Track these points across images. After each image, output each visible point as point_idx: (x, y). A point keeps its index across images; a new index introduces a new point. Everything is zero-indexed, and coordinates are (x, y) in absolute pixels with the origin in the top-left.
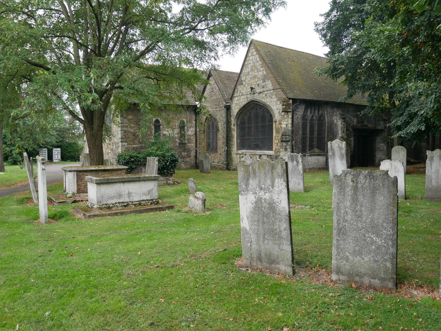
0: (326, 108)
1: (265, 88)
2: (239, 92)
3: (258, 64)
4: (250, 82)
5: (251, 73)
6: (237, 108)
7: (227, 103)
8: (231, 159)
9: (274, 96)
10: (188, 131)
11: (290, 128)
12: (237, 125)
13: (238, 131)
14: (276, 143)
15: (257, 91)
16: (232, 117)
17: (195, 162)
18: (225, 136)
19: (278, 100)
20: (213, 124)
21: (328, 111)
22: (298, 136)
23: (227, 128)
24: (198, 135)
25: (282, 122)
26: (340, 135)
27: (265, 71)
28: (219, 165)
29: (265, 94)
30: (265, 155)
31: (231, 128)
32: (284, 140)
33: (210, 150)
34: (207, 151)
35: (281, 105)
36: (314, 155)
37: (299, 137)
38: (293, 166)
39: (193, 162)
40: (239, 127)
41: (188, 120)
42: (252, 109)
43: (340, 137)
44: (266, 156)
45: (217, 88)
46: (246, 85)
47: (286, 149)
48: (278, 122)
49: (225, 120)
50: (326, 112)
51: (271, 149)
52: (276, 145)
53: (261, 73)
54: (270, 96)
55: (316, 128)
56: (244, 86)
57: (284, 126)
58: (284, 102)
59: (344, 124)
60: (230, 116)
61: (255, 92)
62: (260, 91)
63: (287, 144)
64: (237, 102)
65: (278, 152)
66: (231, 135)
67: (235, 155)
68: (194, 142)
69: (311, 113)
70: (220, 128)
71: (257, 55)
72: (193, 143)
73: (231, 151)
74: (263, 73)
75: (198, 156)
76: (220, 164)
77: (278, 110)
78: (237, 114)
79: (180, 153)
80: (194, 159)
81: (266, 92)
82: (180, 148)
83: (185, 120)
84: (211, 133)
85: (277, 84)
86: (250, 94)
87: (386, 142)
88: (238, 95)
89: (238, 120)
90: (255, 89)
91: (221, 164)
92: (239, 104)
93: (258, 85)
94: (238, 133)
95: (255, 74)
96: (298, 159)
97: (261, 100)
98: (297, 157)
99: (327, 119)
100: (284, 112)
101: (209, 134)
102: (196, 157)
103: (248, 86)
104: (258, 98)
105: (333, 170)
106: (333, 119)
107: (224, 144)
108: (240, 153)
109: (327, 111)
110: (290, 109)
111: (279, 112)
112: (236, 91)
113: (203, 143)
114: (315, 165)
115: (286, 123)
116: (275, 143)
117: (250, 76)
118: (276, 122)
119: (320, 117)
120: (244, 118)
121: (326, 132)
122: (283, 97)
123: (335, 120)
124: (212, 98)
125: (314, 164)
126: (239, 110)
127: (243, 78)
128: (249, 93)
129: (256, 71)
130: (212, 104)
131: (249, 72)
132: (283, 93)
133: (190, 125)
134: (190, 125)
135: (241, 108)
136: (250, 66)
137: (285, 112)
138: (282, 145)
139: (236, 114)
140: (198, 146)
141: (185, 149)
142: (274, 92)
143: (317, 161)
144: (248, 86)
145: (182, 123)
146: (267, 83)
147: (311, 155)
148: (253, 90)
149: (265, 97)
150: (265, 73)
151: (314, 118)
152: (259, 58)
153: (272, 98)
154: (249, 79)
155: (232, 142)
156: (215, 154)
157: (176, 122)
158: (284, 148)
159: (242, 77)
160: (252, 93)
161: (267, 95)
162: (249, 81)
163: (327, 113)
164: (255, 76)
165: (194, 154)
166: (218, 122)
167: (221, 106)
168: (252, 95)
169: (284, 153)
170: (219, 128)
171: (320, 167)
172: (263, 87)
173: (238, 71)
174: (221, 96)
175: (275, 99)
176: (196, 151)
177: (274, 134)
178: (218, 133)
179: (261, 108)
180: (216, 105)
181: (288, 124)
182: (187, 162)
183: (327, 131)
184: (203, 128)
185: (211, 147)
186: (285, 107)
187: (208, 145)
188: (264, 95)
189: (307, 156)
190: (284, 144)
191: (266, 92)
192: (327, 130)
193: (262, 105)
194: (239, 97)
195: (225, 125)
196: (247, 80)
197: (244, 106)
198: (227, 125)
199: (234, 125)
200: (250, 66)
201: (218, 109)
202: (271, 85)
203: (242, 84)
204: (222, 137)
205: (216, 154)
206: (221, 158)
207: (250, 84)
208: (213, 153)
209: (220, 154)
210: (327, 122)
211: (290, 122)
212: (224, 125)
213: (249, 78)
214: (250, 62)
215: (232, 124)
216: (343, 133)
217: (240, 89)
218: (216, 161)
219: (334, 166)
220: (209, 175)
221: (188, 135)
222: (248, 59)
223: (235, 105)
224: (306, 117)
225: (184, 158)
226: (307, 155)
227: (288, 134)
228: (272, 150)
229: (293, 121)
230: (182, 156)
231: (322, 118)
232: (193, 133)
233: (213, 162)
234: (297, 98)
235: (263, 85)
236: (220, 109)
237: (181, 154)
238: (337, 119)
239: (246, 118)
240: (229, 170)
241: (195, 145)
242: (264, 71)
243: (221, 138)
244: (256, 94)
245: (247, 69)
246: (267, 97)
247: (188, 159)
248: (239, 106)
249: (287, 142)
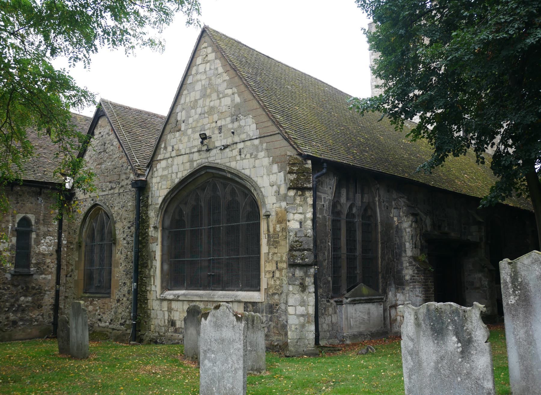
0: (378, 189)
1: (239, 135)
2: (170, 149)
3: (219, 81)
4: (200, 124)
5: (200, 102)
6: (163, 187)
7: (139, 175)
8: (146, 312)
9: (262, 154)
10: (38, 243)
11: (310, 232)
12: (163, 229)
13: (166, 243)
14: (269, 272)
15: (218, 144)
16: (150, 208)
17: (52, 320)
18: (131, 255)
19: (274, 162)
20: (103, 227)
21: (382, 198)
22: (324, 254)
23: (137, 236)
24: (64, 255)
25: (291, 216)
26: (409, 253)
27: (239, 96)
28: (114, 327)
29: (237, 150)
30: (239, 302)
31: (148, 235)
32: (299, 261)
33: (93, 290)
34: (86, 293)
35: (282, 174)
36: (360, 302)
37: (326, 255)
38: (442, 358)
39: (48, 320)
40: (167, 232)
41: (41, 218)
42: (203, 189)
43: (411, 257)
44: (242, 306)
45: (116, 142)
46: (189, 131)
47: (303, 287)
48: (273, 218)
49: (132, 216)
50: (377, 199)
51: (256, 287)
52: (268, 276)
53: (227, 101)
54: (251, 155)
55: (359, 236)
56: (185, 133)
57: (294, 225)
58: (293, 164)
59: (416, 229)
60: (147, 206)
61: (211, 147)
62: (224, 142)
63: (306, 274)
64: (165, 173)
65: (274, 294)
66: (148, 252)
67: (158, 302)
68: (54, 270)
69: (348, 199)
70: (120, 236)
71: (218, 61)
72: (51, 273)
73: (146, 291)
74: (233, 100)
75: (61, 306)
76: (116, 325)
77: (275, 187)
78: (164, 200)
79: (13, 297)
80: (52, 312)
81: (241, 145)
82: (16, 286)
83: (32, 218)
84: (97, 250)
85: (270, 123)
86: (199, 151)
87: (486, 269)
88: (168, 155)
89: (166, 217)
90: (213, 140)
91: (118, 327)
92: (169, 176)
93: (220, 129)
94: (166, 248)
95: (212, 104)
96: (469, 326)
97: (228, 164)
98: (465, 319)
99: (380, 214)
100: (293, 189)
101: (90, 251)
102: (56, 307)
103: (193, 132)
104: (218, 161)
105: (522, 358)
106: (392, 216)
107: (129, 276)
108: (171, 297)
109: (379, 196)
110: (309, 182)
111: (278, 192)
112: (163, 146)
113: (76, 273)
114: (362, 326)
115: (298, 217)
116: (266, 272)
117: (199, 110)
118: (268, 216)
119: (366, 210)
120: (181, 211)
121: (380, 246)
122: (289, 153)
123: (395, 219)
124: (103, 166)
125: (360, 323)
126: (168, 190)
127: (181, 116)
128: (195, 150)
129: (214, 96)
130: (102, 180)
131: (196, 101)
132: (288, 144)
133: (45, 229)
134: (45, 229)
135: (173, 185)
136: (198, 87)
137: (297, 189)
138: (294, 275)
139: (160, 200)
140: (63, 280)
141: (28, 288)
142: (261, 143)
143: (366, 317)
144: (193, 132)
145: (25, 221)
146: (242, 123)
147: (354, 302)
148: (205, 142)
149: (238, 158)
150: (237, 99)
151: (354, 210)
152: (223, 66)
153: (256, 158)
154: (197, 116)
155: (150, 270)
156: (104, 300)
157: (8, 221)
158: (297, 282)
159: (179, 114)
160: (205, 148)
161: (244, 152)
162: (197, 121)
163: (379, 200)
164: (212, 108)
165: (52, 301)
166: (115, 223)
167: (124, 183)
168: (204, 155)
169: (297, 296)
170: (118, 237)
171: (374, 330)
172: (233, 133)
173: (165, 113)
174: (124, 159)
175: (266, 161)
176: (57, 293)
177: (264, 248)
178: (113, 248)
179: (225, 186)
180: (110, 182)
181: (305, 222)
182: (31, 320)
183: (382, 243)
184: (77, 237)
185: (96, 283)
186: (294, 176)
187: (89, 277)
188: (236, 152)
189: (347, 303)
190: (299, 273)
191: (241, 145)
192: (382, 240)
193: (229, 176)
194: (170, 160)
195: (133, 229)
196: (191, 120)
197: (183, 181)
198: (137, 229)
199: (155, 228)
200: (198, 87)
201: (117, 191)
202: (254, 126)
203: (179, 130)
204: (123, 257)
205: (107, 300)
206: (120, 311)
207: (198, 129)
208: (99, 298)
209: (118, 301)
210: (381, 222)
211: (310, 215)
212: (129, 228)
213: (196, 114)
214: (199, 77)
215: (152, 226)
216: (415, 248)
217: (173, 142)
218: (107, 317)
219: (530, 343)
220: (84, 364)
221: (39, 253)
222: (194, 71)
223: (158, 179)
224: (339, 208)
225: (23, 311)
226: (345, 301)
227: (306, 247)
228: (259, 290)
229: (314, 214)
230: (20, 306)
231: (369, 213)
232: (51, 248)
233: (100, 320)
234: (322, 157)
235: (232, 128)
236: (121, 191)
237: (18, 300)
238: (399, 216)
239: (187, 211)
240: (141, 341)
241: (55, 278)
242: (236, 95)
243: (121, 261)
244: (214, 152)
245: (193, 94)
246: (243, 156)
247: (35, 314)
248: (169, 182)
249: (304, 266)
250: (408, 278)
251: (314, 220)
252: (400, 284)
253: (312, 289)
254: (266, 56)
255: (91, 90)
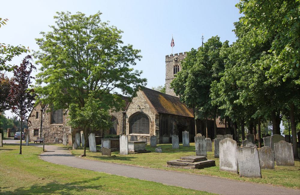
53: (143, 100)
88: (130, 108)
129: (141, 99)
161: (147, 110)
177: (150, 127)
188: (145, 110)
250: (173, 133)
251: (159, 123)
252: (172, 134)
253: (159, 134)
254: (149, 182)
255: (23, 59)
